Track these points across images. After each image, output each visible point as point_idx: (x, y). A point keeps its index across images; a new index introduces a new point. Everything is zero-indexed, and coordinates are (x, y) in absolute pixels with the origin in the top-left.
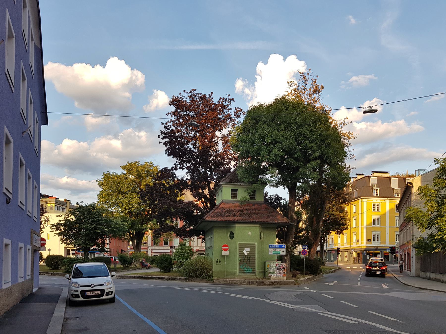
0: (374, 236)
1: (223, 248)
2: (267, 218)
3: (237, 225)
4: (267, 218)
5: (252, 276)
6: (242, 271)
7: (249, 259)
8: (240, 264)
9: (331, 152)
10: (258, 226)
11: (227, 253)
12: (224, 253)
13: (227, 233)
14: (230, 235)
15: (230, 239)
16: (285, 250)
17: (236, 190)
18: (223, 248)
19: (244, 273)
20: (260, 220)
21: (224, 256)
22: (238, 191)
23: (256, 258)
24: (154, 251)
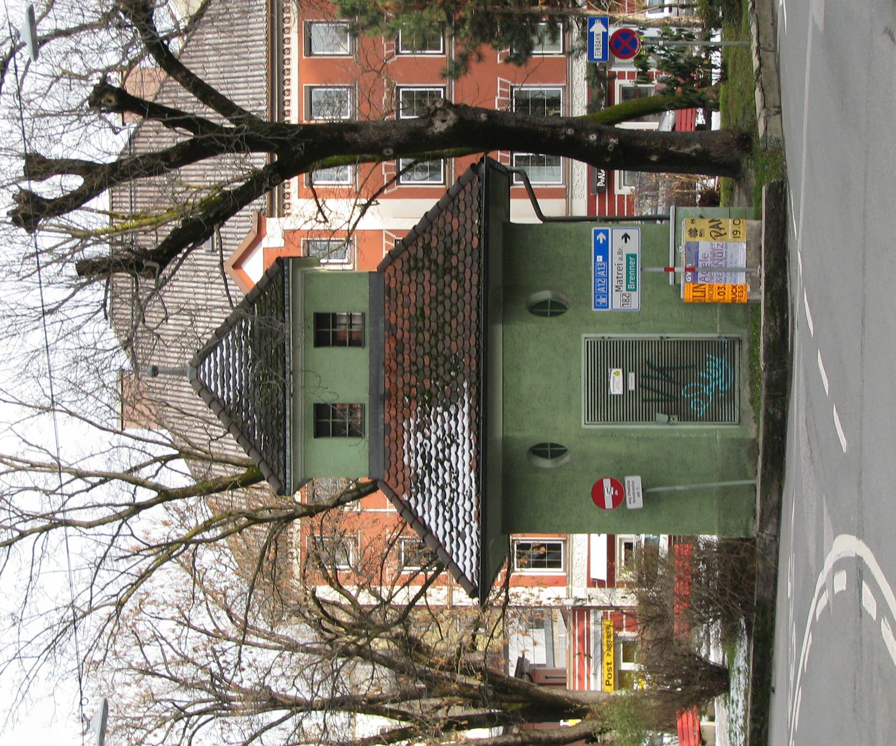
0: (634, 501)
1: (609, 503)
2: (461, 283)
3: (499, 434)
4: (461, 283)
5: (742, 358)
6: (720, 407)
7: (661, 370)
8: (687, 416)
9: (20, 256)
10: (499, 329)
11: (634, 484)
12: (635, 501)
13: (538, 470)
14: (544, 455)
15: (566, 459)
16: (616, 233)
17: (321, 410)
18: (609, 503)
19: (730, 395)
20: (468, 313)
21: (648, 497)
22: (326, 398)
23: (656, 336)
24: (600, 573)
